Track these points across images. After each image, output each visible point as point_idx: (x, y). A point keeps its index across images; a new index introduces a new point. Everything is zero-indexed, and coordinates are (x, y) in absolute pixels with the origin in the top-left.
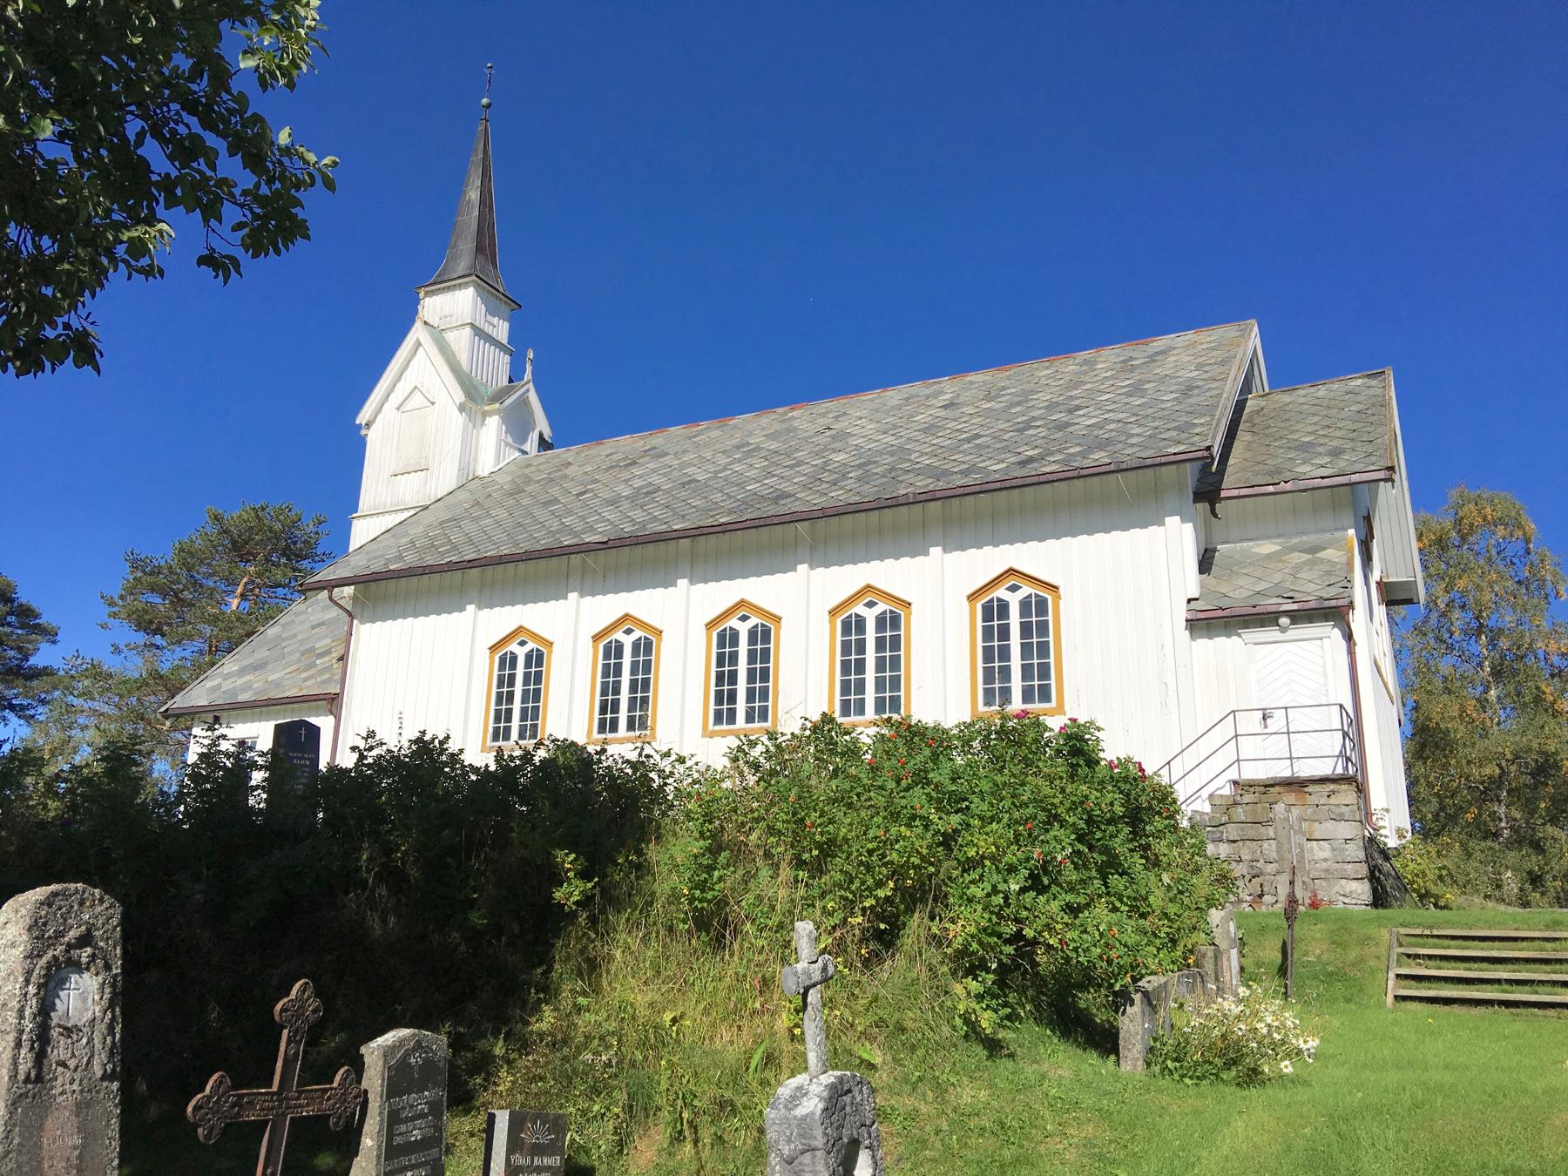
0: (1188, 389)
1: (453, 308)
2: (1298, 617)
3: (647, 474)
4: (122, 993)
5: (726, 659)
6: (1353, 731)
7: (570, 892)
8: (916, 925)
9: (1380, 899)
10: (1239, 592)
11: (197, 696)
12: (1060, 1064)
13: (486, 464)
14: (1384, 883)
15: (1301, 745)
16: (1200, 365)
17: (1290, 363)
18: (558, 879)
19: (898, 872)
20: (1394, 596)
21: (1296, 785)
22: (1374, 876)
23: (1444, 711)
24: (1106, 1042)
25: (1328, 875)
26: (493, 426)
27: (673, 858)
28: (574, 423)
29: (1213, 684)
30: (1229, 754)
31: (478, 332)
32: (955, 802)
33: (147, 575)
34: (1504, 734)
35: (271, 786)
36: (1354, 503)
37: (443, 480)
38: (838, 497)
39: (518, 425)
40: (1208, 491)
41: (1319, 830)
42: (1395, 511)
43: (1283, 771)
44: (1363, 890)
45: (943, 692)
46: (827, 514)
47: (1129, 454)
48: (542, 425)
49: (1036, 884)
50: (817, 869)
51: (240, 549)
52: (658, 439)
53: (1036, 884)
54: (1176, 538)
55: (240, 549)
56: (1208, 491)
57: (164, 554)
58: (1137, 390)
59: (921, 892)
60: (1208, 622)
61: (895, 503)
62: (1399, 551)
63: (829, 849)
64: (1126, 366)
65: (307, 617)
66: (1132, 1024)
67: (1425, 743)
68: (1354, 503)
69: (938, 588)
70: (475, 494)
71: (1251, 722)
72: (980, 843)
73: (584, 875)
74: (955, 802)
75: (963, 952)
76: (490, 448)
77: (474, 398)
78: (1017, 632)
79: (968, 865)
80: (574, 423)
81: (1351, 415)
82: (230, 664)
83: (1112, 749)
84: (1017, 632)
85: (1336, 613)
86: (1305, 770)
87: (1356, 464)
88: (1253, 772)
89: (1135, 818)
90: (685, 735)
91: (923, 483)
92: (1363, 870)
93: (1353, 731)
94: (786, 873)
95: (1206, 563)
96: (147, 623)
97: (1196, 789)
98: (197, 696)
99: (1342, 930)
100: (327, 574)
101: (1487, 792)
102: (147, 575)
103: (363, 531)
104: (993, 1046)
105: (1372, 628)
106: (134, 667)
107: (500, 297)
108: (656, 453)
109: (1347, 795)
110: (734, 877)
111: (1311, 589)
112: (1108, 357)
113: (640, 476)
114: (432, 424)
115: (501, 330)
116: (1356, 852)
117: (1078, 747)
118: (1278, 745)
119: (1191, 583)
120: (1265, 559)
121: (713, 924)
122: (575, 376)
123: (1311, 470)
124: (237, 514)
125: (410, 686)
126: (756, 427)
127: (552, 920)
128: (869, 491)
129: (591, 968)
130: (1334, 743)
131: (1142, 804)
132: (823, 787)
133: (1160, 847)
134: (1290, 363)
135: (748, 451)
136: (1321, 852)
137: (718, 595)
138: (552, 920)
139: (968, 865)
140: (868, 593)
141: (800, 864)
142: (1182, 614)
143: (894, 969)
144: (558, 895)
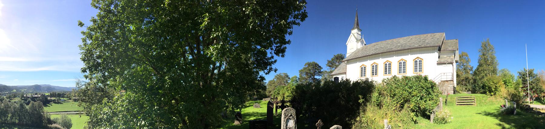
0: (438, 39)
2: (448, 63)
3: (377, 47)
6: (453, 76)
7: (361, 101)
8: (406, 105)
9: (454, 93)
10: (442, 61)
11: (333, 73)
12: (423, 122)
13: (359, 47)
14: (455, 92)
15: (448, 77)
16: (439, 37)
17: (448, 37)
18: (360, 99)
19: (404, 98)
20: (457, 62)
21: (447, 81)
23: (459, 73)
24: (428, 118)
26: (360, 43)
27: (375, 95)
28: (368, 42)
29: (438, 69)
32: (410, 88)
33: (329, 62)
34: (464, 76)
35: (189, 122)
36: (454, 52)
37: (355, 49)
38: (399, 49)
39: (362, 43)
40: (440, 50)
42: (457, 53)
43: (446, 80)
45: (410, 72)
46: (397, 51)
47: (431, 45)
48: (365, 43)
49: (421, 99)
50: (393, 98)
51: (337, 58)
52: (378, 43)
53: (421, 99)
54: (436, 54)
55: (337, 58)
56: (440, 50)
57: (330, 60)
58: (432, 38)
59: (407, 101)
60: (439, 64)
61: (405, 50)
62: (457, 58)
63: (395, 95)
64: (431, 36)
65: (343, 64)
66: (432, 116)
67: (458, 76)
68: (454, 52)
69: (410, 59)
70: (358, 51)
71: (443, 74)
72: (414, 93)
73: (363, 98)
74: (410, 88)
75: (412, 109)
76: (359, 46)
77: (357, 40)
78: (418, 64)
79: (413, 96)
80: (368, 42)
81: (452, 43)
82: (336, 70)
83: (429, 79)
84: (418, 64)
85: (452, 63)
86: (448, 80)
87: (454, 48)
89: (432, 87)
90: (378, 79)
91: (409, 47)
93: (453, 76)
94: (389, 98)
95: (439, 57)
96: (330, 66)
97: (437, 82)
98: (333, 73)
99: (452, 96)
100: (344, 60)
101: (463, 80)
102: (329, 62)
103: (347, 55)
104: (415, 122)
105: (455, 64)
106: (329, 71)
107: (360, 30)
108: (377, 45)
109: (452, 82)
110: (382, 98)
111: (450, 61)
112: (429, 35)
113: (375, 47)
114: (353, 44)
117: (426, 79)
118: (445, 77)
119: (438, 59)
120: (445, 57)
121: (380, 105)
122: (368, 37)
123: (450, 48)
124: (336, 55)
125: (352, 73)
126: (389, 41)
127: (359, 105)
128: (402, 48)
129: (364, 111)
130: (451, 77)
131: (433, 86)
132: (394, 86)
133: (435, 90)
134: (448, 37)
136: (449, 88)
138: (359, 105)
139: (413, 96)
141: (391, 96)
143: (403, 111)
144: (359, 101)
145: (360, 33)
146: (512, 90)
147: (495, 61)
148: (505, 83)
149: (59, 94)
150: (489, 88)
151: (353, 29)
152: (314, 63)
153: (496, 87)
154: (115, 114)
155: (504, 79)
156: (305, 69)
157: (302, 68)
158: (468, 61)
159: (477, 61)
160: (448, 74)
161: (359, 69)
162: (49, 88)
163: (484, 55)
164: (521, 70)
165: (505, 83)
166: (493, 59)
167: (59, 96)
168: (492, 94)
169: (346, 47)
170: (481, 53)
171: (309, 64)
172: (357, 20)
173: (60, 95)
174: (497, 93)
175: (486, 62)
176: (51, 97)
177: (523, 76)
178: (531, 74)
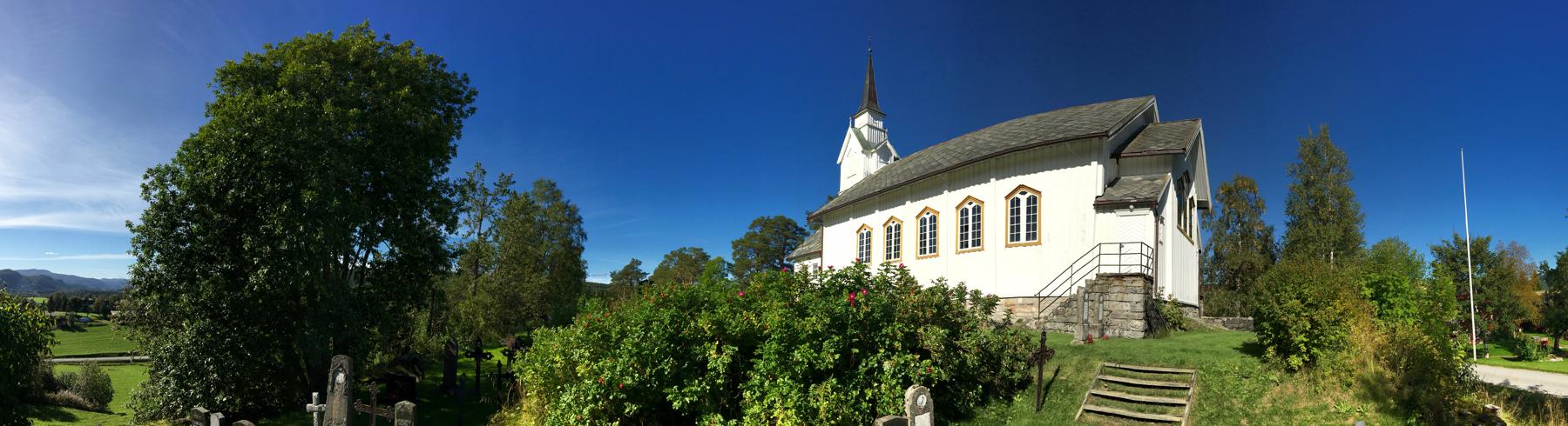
1: (863, 120)
4: (1557, 336)
5: (964, 221)
10: (1117, 194)
21: (1119, 277)
22: (1147, 318)
25: (1127, 318)
28: (903, 152)
30: (1096, 262)
31: (870, 126)
37: (860, 178)
40: (1116, 155)
41: (1126, 297)
43: (1115, 270)
44: (1140, 324)
48: (894, 154)
70: (870, 179)
76: (874, 164)
85: (1156, 207)
86: (1124, 270)
88: (1103, 270)
92: (1142, 315)
107: (877, 114)
111: (1145, 193)
115: (880, 125)
116: (1140, 307)
122: (902, 134)
135: (946, 151)
137: (959, 195)
140: (1022, 188)
142: (1093, 201)
145: (880, 125)
146: (1409, 328)
147: (1351, 206)
148: (1376, 297)
149: (75, 300)
150: (1280, 327)
151: (855, 114)
152: (783, 218)
153: (1315, 324)
154: (178, 349)
155: (1376, 277)
156: (750, 236)
157: (740, 233)
158: (1257, 209)
159: (1284, 207)
160: (1105, 249)
161: (855, 239)
162: (44, 282)
163: (1308, 184)
164: (1443, 238)
165: (1376, 297)
166: (1343, 199)
167: (79, 304)
168: (1295, 361)
169: (837, 169)
170: (1299, 181)
171: (764, 223)
172: (872, 83)
173: (79, 305)
174: (1322, 357)
175: (1325, 223)
176: (51, 310)
177: (1451, 259)
178: (1479, 249)
